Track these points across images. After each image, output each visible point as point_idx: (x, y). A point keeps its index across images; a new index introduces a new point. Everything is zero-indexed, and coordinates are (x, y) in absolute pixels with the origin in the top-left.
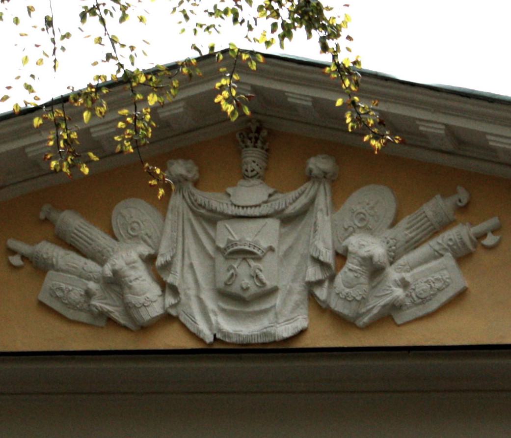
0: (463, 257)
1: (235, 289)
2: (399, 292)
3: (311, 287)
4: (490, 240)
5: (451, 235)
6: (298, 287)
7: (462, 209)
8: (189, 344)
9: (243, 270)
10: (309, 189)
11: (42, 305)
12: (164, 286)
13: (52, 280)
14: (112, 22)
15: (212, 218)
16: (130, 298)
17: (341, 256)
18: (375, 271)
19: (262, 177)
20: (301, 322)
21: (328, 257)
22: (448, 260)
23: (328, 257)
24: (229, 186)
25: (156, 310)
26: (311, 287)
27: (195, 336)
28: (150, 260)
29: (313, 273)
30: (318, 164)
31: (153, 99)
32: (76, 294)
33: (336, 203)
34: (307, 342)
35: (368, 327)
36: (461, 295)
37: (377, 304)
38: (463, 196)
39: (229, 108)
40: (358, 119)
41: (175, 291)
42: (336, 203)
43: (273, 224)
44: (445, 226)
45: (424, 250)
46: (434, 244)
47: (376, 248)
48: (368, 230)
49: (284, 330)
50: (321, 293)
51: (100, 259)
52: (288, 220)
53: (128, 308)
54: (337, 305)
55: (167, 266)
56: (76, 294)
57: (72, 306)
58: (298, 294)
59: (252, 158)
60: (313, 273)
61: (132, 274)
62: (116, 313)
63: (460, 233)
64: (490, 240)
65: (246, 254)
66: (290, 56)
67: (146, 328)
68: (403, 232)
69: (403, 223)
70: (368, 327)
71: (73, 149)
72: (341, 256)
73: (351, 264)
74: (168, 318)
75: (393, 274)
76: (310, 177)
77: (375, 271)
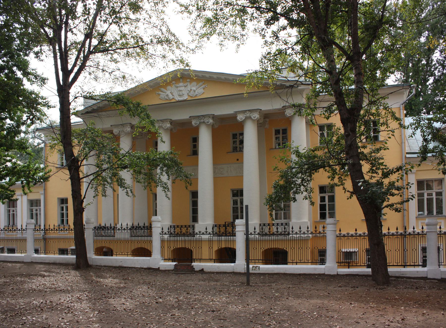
0: (204, 89)
1: (180, 94)
2: (197, 93)
3: (188, 93)
4: (207, 86)
5: (202, 87)
6: (187, 94)
7: (204, 83)
8: (176, 101)
9: (181, 92)
10: (187, 83)
11: (160, 99)
12: (172, 95)
13: (161, 96)
14: (166, 68)
15: (177, 87)
16: (169, 97)
17: (191, 90)
18: (195, 91)
19: (182, 82)
20: (187, 97)
21: (190, 90)
22: (202, 89)
23: (190, 90)
24: (68, 69)
25: (172, 98)
26: (188, 93)
27: (176, 100)
28: (171, 92)
29: (188, 92)
30: (188, 80)
31: (171, 76)
32: (163, 97)
33: (190, 84)
34: (188, 100)
35: (194, 97)
36: (204, 93)
37: (195, 95)
38: (204, 82)
39: (179, 76)
40: (193, 76)
41: (174, 95)
42: (190, 84)
43: (184, 87)
44: (202, 85)
45: (200, 88)
46: (201, 87)
47: (194, 88)
48: (194, 87)
49: (185, 98)
50: (189, 94)
51: (165, 93)
52: (185, 86)
53: (169, 98)
54: (191, 95)
55: (173, 93)
56: (163, 97)
57: (163, 98)
58: (187, 94)
59: (181, 80)
60: (188, 92)
61: (169, 94)
62: (168, 99)
63: (203, 86)
64: (207, 86)
65: (181, 91)
66: (416, 207)
67: (171, 100)
68: (197, 86)
69: (198, 85)
70: (194, 97)
71: (163, 82)
72: (191, 90)
73: (192, 91)
74: (173, 98)
75: (196, 91)
76: (187, 82)
77: (195, 91)
